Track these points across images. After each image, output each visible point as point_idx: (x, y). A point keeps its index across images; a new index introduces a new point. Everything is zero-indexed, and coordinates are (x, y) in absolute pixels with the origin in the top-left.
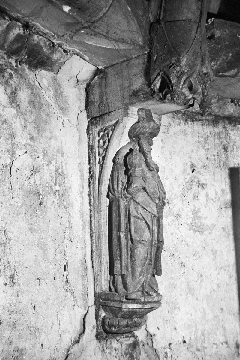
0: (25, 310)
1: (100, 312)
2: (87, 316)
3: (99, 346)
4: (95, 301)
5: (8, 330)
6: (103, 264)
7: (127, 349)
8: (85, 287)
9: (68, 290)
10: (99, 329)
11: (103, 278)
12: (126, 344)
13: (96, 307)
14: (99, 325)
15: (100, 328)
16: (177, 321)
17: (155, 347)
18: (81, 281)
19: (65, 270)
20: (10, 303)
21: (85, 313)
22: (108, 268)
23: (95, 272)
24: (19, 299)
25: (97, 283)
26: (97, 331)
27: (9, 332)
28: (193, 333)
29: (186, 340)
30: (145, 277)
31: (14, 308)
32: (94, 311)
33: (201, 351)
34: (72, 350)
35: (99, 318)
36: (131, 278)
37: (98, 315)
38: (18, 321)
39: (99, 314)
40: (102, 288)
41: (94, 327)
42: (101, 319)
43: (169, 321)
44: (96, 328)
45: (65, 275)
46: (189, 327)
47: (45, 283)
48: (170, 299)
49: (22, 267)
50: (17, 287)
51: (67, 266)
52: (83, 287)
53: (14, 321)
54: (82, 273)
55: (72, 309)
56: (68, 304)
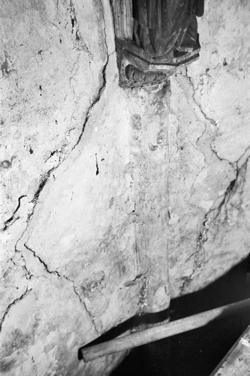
0: (29, 96)
1: (123, 61)
2: (107, 67)
3: (124, 93)
4: (116, 44)
5: (13, 125)
6: (124, 5)
7: (155, 98)
8: (102, 33)
9: (80, 48)
10: (123, 79)
11: (125, 22)
12: (154, 93)
13: (118, 54)
14: (122, 74)
15: (123, 77)
16: (220, 42)
17: (189, 75)
18: (96, 29)
19: (73, 26)
20: (9, 97)
21: (105, 64)
22: (132, 10)
23: (114, 11)
24: (20, 88)
25: (117, 26)
26: (120, 80)
27: (22, 24)
28: (238, 51)
29: (227, 62)
30: (179, 34)
31: (15, 100)
32: (115, 59)
33: (244, 70)
34: (92, 112)
35: (122, 68)
36: (160, 34)
37: (121, 65)
38: (23, 112)
39: (122, 63)
40: (124, 35)
41: (116, 76)
42: (124, 69)
43: (209, 44)
44: (118, 77)
45: (74, 32)
46: (234, 46)
47: (50, 53)
48: (213, 17)
49: (15, 47)
50: (13, 75)
51: (76, 20)
52: (100, 34)
53: (19, 113)
54: (98, 18)
55: (88, 68)
56: (82, 65)
